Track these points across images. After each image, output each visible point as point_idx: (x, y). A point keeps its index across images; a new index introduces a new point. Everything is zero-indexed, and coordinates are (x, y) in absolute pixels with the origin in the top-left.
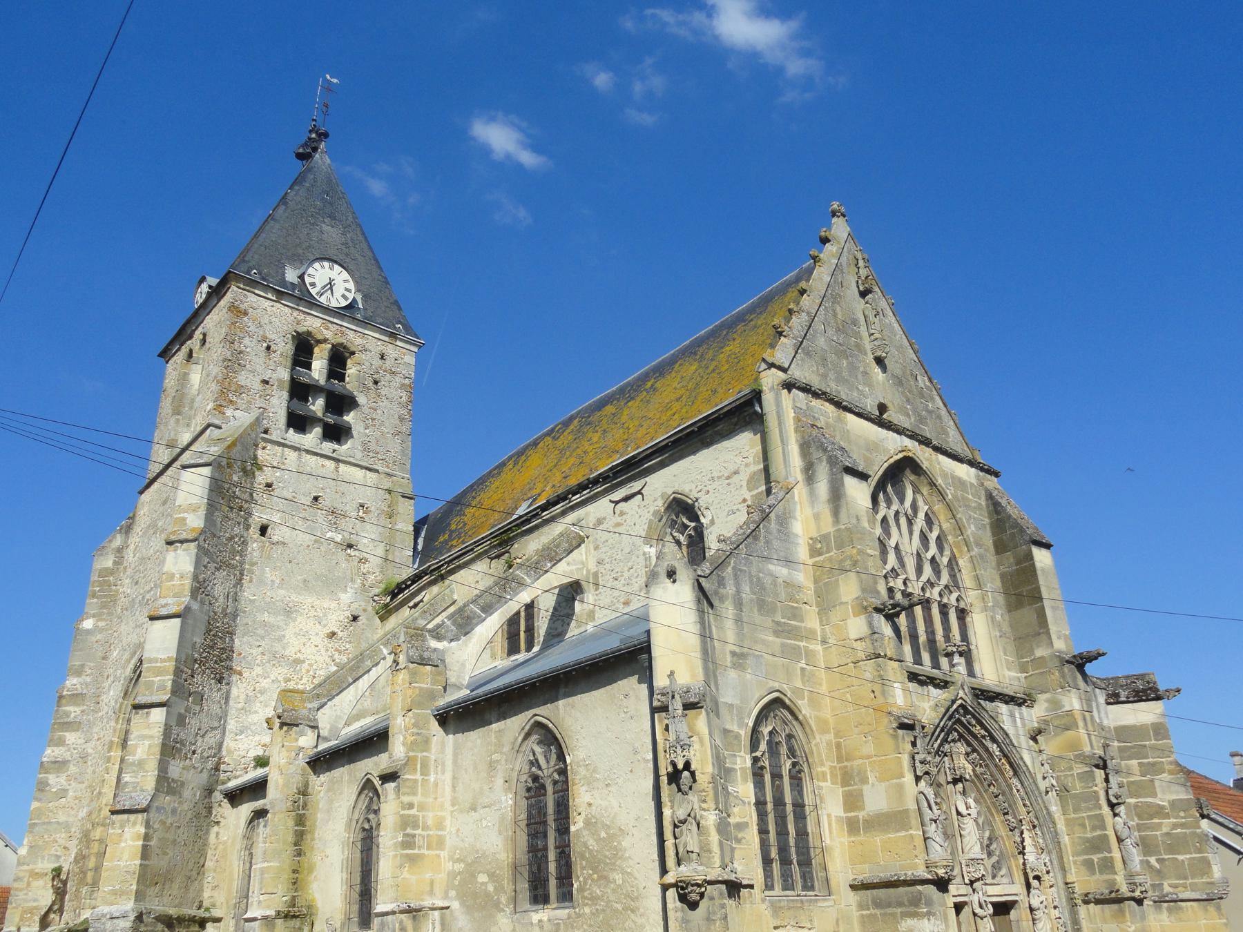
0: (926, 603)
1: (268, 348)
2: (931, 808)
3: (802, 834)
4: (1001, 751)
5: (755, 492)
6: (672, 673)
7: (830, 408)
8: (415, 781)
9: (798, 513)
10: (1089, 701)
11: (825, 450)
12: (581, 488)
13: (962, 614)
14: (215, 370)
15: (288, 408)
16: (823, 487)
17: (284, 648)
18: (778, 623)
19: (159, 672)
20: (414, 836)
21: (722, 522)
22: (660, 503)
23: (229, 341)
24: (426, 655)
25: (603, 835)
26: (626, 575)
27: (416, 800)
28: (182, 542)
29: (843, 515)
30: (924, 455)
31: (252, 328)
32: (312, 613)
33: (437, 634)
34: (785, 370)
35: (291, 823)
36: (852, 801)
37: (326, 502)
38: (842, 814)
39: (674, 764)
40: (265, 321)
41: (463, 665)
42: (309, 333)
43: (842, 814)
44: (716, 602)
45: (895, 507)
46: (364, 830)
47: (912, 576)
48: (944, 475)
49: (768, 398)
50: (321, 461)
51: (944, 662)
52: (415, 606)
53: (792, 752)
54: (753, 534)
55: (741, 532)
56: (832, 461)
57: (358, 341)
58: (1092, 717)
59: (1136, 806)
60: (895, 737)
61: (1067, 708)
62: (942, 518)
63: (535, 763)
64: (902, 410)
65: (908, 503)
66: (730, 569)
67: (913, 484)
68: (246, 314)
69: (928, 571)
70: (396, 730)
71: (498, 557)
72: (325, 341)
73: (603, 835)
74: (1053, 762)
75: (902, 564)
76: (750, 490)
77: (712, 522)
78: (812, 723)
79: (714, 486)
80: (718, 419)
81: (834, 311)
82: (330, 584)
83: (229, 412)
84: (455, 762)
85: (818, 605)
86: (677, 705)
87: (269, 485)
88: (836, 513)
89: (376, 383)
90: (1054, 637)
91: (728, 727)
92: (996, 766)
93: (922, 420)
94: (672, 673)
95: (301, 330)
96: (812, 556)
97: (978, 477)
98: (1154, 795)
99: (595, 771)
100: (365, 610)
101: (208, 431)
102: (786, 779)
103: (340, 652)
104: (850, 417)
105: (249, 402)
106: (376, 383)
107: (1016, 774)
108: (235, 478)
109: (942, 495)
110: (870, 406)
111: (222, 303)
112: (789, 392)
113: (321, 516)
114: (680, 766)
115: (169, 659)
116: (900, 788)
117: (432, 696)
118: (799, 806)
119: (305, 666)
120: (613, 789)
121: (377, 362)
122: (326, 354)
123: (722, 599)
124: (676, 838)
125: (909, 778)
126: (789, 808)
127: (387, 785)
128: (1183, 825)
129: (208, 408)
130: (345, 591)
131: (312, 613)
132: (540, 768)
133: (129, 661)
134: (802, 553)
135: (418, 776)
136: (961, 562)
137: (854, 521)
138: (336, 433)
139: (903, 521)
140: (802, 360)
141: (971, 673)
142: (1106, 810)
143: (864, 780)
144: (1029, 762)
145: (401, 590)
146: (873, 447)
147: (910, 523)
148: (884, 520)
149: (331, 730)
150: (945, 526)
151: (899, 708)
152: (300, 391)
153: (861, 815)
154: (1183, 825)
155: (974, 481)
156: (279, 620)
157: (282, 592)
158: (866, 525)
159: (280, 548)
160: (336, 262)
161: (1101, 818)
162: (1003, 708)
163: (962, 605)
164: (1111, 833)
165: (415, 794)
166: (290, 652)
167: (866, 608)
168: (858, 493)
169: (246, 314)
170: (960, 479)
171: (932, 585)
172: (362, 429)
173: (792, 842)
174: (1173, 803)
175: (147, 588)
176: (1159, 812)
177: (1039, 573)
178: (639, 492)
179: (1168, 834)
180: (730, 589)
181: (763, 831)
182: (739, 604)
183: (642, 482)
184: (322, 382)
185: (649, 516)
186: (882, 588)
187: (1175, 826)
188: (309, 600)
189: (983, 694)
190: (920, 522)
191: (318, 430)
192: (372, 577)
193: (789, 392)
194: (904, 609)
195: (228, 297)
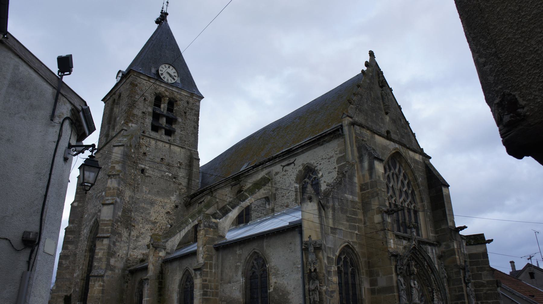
0: (403, 209)
1: (145, 99)
2: (402, 285)
3: (355, 294)
4: (428, 263)
5: (339, 165)
6: (310, 236)
7: (368, 133)
8: (207, 271)
9: (356, 175)
10: (460, 245)
11: (367, 150)
12: (269, 160)
13: (416, 212)
14: (124, 108)
15: (152, 123)
16: (366, 164)
17: (150, 217)
18: (348, 217)
19: (106, 225)
20: (207, 291)
21: (327, 176)
22: (301, 167)
23: (130, 96)
24: (211, 224)
25: (281, 294)
26: (287, 195)
27: (208, 278)
28: (114, 175)
29: (374, 176)
30: (402, 150)
31: (139, 91)
32: (161, 204)
33: (214, 216)
34: (351, 118)
35: (157, 284)
36: (373, 283)
37: (166, 161)
38: (369, 287)
39: (310, 270)
40: (144, 89)
41: (224, 229)
42: (160, 93)
43: (369, 287)
44: (326, 209)
45: (392, 171)
46: (185, 288)
47: (398, 199)
48: (411, 158)
49: (346, 129)
50: (164, 144)
51: (409, 230)
52: (201, 203)
53: (352, 265)
54: (340, 183)
55: (335, 181)
56: (370, 154)
57: (179, 96)
58: (461, 251)
59: (474, 283)
60: (390, 259)
61: (452, 248)
62: (409, 175)
63: (253, 267)
64: (395, 133)
65: (397, 170)
66: (331, 196)
67: (399, 162)
68: (137, 85)
69: (404, 196)
70: (200, 252)
71: (235, 185)
72: (166, 96)
73: (281, 294)
74: (446, 268)
75: (394, 193)
76: (337, 164)
77: (322, 176)
78: (360, 254)
79: (323, 161)
80: (326, 136)
81: (370, 94)
82: (167, 193)
83: (130, 125)
84: (222, 265)
85: (363, 210)
86: (311, 249)
87: (145, 154)
88: (371, 175)
89: (185, 113)
90: (449, 221)
91: (329, 256)
92: (425, 269)
93: (403, 137)
94: (310, 236)
95: (157, 92)
96: (361, 191)
97: (423, 159)
98: (482, 279)
99: (278, 270)
100: (180, 203)
101: (122, 132)
102: (349, 275)
103: (171, 220)
104: (376, 136)
105: (137, 121)
106: (185, 113)
107: (432, 272)
108: (132, 151)
109: (410, 166)
110: (383, 131)
111: (128, 81)
112: (354, 126)
113: (164, 168)
114: (313, 270)
115: (110, 220)
116: (392, 278)
117: (213, 240)
118: (354, 285)
119: (158, 224)
120: (285, 277)
121: (186, 105)
122: (167, 102)
123: (328, 208)
124: (310, 296)
125: (394, 275)
126: (350, 285)
127: (196, 272)
128: (491, 290)
129: (122, 122)
130: (173, 196)
131: (161, 204)
132: (255, 268)
133: (91, 219)
134: (357, 189)
135: (208, 270)
136: (416, 192)
137: (377, 178)
138: (169, 133)
139: (395, 176)
140: (358, 113)
141: (418, 234)
142: (464, 285)
143: (378, 275)
144: (437, 268)
145: (195, 196)
146: (385, 148)
147: (398, 178)
148: (388, 176)
149: (171, 250)
150: (410, 178)
151: (392, 249)
152: (156, 116)
153: (376, 287)
154: (491, 290)
155: (421, 161)
156: (148, 206)
157: (149, 196)
158: (382, 179)
159: (149, 178)
160: (171, 65)
161: (462, 288)
162: (429, 248)
163: (416, 209)
164: (465, 293)
165: (207, 276)
166: (153, 219)
167: (381, 211)
168: (379, 167)
169: (137, 85)
170: (416, 160)
171: (405, 202)
172: (179, 132)
173: (351, 297)
174: (488, 282)
175: (98, 192)
176: (483, 285)
177: (444, 196)
178: (293, 163)
179: (485, 293)
180: (331, 204)
181: (341, 293)
182: (334, 209)
183: (294, 159)
184: (165, 112)
185: (297, 172)
186: (387, 204)
187: (488, 290)
188: (160, 199)
189: (421, 242)
190: (401, 177)
191: (163, 131)
192: (183, 190)
193: (354, 126)
194: (395, 212)
195: (130, 79)
